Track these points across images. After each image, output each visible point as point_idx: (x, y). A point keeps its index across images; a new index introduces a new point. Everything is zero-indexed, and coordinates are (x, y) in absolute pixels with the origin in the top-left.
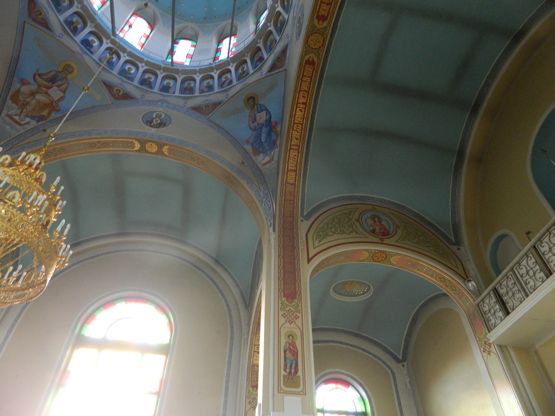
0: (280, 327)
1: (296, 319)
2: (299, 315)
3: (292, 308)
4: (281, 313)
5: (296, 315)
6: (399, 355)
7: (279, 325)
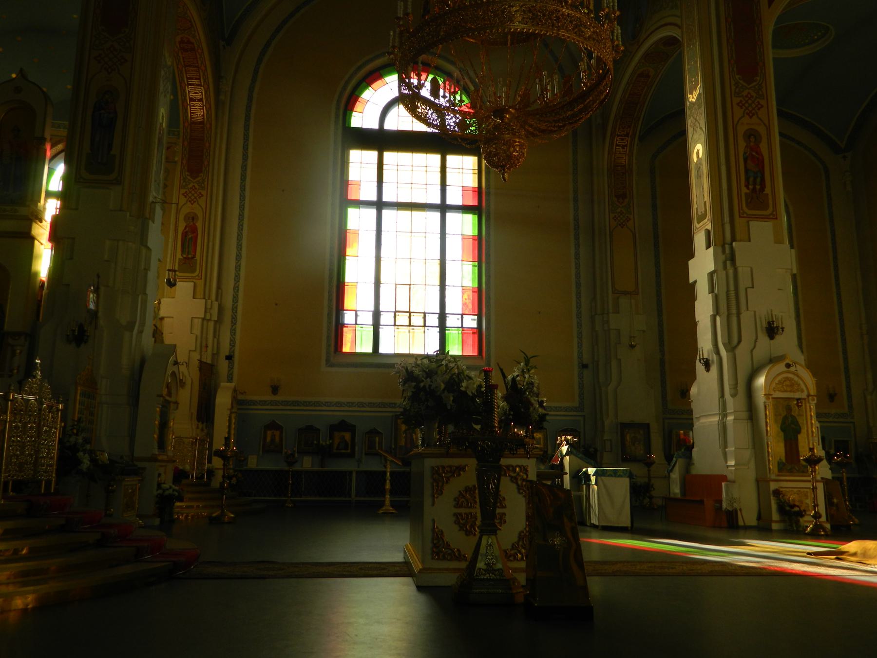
0: (735, 123)
1: (759, 109)
2: (204, 192)
5: (200, 193)
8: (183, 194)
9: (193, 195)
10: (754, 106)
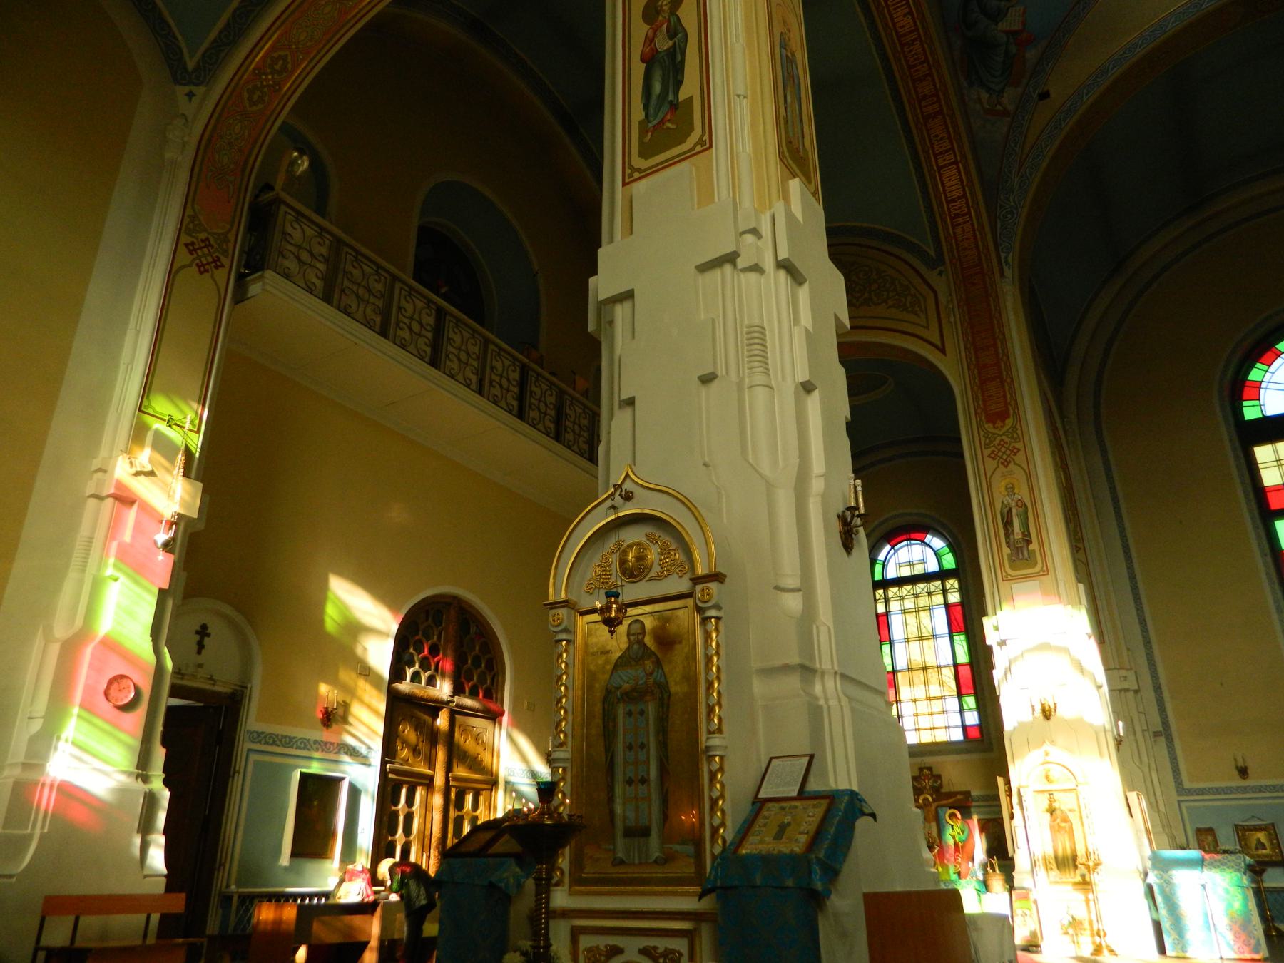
0: (988, 476)
1: (1015, 454)
2: (1017, 445)
3: (1004, 437)
4: (185, 239)
6: (191, 57)
7: (175, 265)
8: (989, 456)
9: (1004, 453)
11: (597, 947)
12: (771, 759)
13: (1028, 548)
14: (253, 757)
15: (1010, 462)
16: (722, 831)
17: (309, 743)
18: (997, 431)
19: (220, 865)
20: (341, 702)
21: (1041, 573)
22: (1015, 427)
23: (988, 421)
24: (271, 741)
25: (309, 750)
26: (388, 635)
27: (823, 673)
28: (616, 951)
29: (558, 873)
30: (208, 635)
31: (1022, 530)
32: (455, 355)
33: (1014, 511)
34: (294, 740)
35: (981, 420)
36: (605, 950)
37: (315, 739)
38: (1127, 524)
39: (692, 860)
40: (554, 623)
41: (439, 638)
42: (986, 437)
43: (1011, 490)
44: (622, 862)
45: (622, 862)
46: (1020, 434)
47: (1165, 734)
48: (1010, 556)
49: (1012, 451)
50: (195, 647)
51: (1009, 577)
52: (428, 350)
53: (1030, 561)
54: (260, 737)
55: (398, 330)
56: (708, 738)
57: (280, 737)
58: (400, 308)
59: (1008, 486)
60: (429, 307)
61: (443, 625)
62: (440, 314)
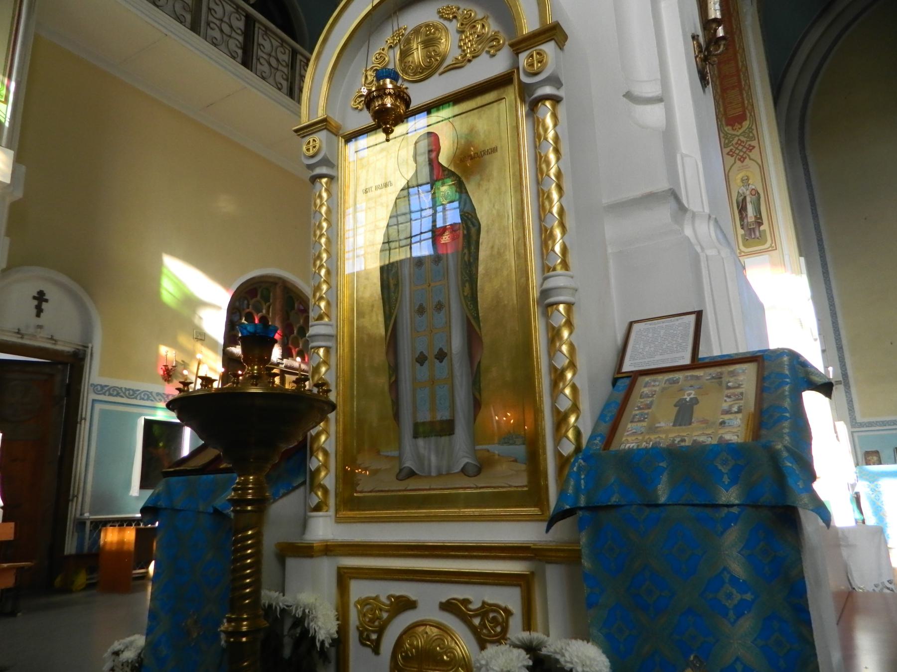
1: (751, 151)
5: (750, 145)
8: (728, 154)
10: (741, 154)
11: (376, 598)
12: (631, 324)
13: (759, 228)
14: (98, 407)
15: (746, 158)
16: (572, 419)
17: (152, 395)
18: (735, 133)
19: (74, 497)
20: (180, 361)
21: (770, 249)
22: (751, 128)
23: (727, 125)
24: (115, 393)
25: (152, 400)
26: (219, 308)
27: (694, 215)
28: (405, 604)
29: (320, 493)
30: (46, 301)
31: (755, 214)
32: (265, 59)
33: (748, 199)
34: (138, 393)
35: (722, 124)
36: (388, 602)
37: (157, 391)
38: (822, 223)
39: (523, 467)
40: (308, 154)
41: (268, 312)
42: (726, 139)
43: (745, 181)
44: (411, 474)
45: (411, 474)
46: (756, 136)
47: (844, 382)
48: (743, 236)
49: (748, 149)
50: (34, 311)
51: (743, 254)
52: (240, 52)
53: (761, 239)
54: (103, 389)
55: (209, 29)
56: (545, 279)
57: (124, 390)
58: (209, 9)
59: (744, 178)
60: (237, 12)
61: (271, 301)
62: (250, 21)
